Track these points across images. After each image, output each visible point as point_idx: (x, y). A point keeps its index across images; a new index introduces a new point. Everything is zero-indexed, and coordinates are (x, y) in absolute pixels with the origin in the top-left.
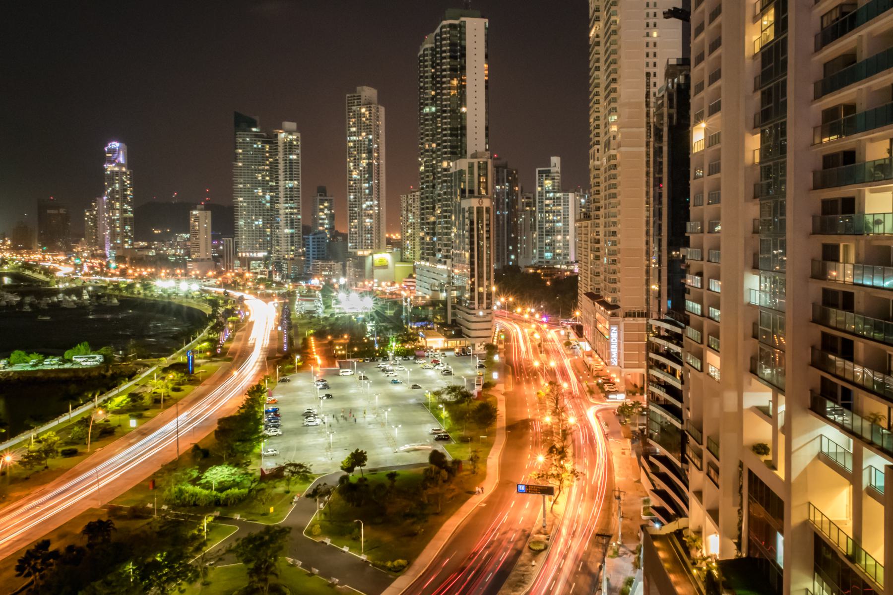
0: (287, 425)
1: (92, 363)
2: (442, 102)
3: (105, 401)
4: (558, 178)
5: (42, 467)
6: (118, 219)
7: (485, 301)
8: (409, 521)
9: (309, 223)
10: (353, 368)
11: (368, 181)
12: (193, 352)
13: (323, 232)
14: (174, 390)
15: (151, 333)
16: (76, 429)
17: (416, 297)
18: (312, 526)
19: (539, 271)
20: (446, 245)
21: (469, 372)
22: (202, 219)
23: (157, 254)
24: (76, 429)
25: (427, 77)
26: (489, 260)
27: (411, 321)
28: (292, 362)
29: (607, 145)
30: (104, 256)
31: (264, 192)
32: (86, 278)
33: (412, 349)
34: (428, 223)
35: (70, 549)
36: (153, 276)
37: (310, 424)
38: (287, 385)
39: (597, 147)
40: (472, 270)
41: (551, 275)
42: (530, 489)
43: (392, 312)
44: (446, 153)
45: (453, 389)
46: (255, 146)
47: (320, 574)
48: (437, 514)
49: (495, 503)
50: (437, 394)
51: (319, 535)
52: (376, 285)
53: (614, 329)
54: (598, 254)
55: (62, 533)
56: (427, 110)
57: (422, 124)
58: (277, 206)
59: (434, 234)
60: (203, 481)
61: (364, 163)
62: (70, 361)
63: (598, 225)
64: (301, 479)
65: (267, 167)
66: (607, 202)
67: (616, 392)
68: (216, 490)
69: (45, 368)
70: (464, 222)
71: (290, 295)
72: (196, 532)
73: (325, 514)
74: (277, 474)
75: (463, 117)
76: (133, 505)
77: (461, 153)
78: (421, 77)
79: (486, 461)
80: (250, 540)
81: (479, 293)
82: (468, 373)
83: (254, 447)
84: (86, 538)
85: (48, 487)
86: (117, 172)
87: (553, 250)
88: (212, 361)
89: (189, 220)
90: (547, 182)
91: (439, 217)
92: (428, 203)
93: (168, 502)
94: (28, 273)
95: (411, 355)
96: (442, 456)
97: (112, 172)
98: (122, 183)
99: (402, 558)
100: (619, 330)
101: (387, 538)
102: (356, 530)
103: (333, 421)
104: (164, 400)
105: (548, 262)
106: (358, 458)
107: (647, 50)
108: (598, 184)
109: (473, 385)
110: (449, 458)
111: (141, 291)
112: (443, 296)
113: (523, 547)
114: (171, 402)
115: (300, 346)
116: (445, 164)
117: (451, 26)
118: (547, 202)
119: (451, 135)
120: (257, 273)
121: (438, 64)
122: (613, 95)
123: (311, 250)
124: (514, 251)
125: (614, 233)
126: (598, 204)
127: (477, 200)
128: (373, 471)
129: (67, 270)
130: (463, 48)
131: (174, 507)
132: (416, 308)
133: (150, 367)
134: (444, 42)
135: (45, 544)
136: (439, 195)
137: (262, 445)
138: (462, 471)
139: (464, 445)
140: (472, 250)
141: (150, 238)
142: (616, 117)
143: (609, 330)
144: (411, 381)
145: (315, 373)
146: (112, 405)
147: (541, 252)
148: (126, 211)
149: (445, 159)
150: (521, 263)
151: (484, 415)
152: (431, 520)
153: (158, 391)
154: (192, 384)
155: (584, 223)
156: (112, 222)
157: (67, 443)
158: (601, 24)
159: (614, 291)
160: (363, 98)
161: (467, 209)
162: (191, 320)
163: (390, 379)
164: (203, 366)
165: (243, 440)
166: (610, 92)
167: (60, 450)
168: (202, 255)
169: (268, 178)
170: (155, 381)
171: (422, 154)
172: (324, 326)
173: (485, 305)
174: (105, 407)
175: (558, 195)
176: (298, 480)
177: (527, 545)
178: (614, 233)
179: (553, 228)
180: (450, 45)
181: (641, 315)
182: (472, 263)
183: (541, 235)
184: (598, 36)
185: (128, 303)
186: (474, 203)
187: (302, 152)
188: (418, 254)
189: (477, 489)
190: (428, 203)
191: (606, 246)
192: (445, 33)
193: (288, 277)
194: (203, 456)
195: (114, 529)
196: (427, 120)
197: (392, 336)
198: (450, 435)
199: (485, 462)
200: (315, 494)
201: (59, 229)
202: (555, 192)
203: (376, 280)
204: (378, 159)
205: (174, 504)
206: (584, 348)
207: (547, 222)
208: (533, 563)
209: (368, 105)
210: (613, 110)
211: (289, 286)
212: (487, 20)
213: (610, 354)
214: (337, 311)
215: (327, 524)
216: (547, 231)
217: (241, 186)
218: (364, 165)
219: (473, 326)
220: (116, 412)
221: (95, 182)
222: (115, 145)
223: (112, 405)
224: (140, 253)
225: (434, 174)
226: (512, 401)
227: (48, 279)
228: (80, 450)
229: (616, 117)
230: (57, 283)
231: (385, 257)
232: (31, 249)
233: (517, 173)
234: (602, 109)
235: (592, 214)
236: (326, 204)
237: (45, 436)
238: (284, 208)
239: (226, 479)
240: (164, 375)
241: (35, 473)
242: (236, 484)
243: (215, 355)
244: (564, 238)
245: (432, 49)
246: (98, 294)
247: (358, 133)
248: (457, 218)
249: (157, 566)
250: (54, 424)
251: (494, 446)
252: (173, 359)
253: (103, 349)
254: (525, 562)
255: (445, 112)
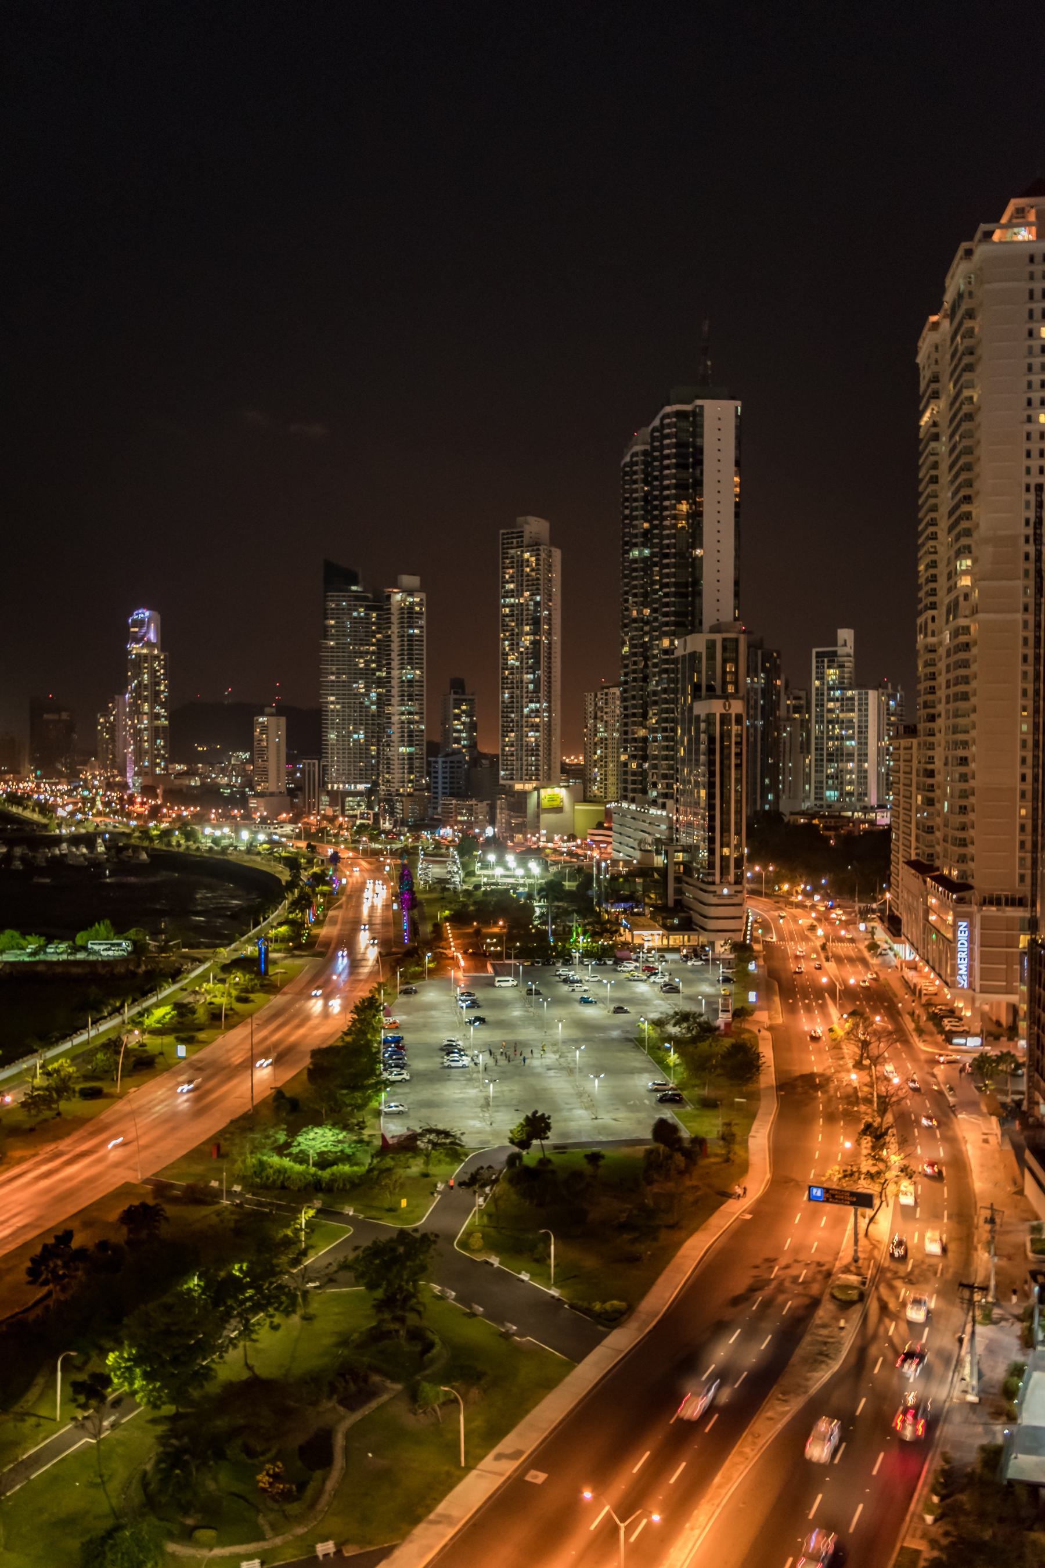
0: (419, 1065)
1: (116, 953)
2: (661, 540)
3: (141, 1014)
4: (849, 665)
5: (53, 1113)
6: (146, 729)
7: (732, 871)
8: (626, 1237)
9: (437, 739)
10: (516, 975)
11: (533, 669)
12: (267, 939)
13: (457, 752)
14: (241, 1000)
15: (199, 908)
16: (100, 1056)
17: (615, 862)
18: (469, 1234)
19: (816, 821)
20: (665, 776)
21: (706, 989)
22: (272, 729)
23: (203, 784)
24: (100, 1056)
25: (636, 500)
26: (738, 802)
27: (607, 901)
28: (419, 963)
29: (953, 609)
30: (124, 786)
31: (368, 687)
32: (98, 819)
33: (612, 947)
34: (635, 740)
35: (103, 1245)
36: (201, 819)
37: (453, 1064)
38: (413, 999)
39: (931, 613)
40: (712, 818)
41: (835, 828)
42: (832, 1196)
43: (575, 884)
44: (667, 624)
45: (683, 1018)
46: (355, 614)
47: (487, 1315)
48: (671, 1227)
49: (768, 1213)
50: (658, 1023)
51: (479, 1251)
52: (543, 839)
53: (963, 924)
54: (931, 795)
55: (87, 1217)
56: (636, 553)
57: (625, 576)
58: (389, 710)
59: (645, 758)
60: (295, 1150)
61: (527, 641)
62: (84, 948)
63: (931, 747)
64: (447, 1155)
65: (372, 648)
66: (950, 706)
67: (966, 1034)
68: (315, 1165)
69: (49, 958)
70: (698, 739)
71: (409, 853)
72: (289, 1233)
73: (490, 1216)
74: (408, 1145)
75: (696, 564)
76: (190, 1181)
77: (693, 624)
78: (626, 500)
79: (747, 1141)
80: (376, 1251)
81: (722, 857)
82: (707, 989)
83: (369, 1099)
84: (124, 1230)
85: (63, 1145)
86: (146, 656)
87: (839, 787)
88: (294, 956)
89: (253, 731)
90: (832, 671)
91: (654, 730)
92: (634, 706)
93: (242, 1179)
94: (14, 809)
95: (610, 957)
96: (674, 1129)
97: (138, 655)
98: (153, 672)
99: (620, 1299)
100: (971, 927)
101: (590, 1262)
102: (541, 1246)
103: (490, 1062)
104: (226, 1016)
105: (829, 806)
106: (536, 1126)
107: (1027, 446)
108: (933, 676)
109: (716, 1011)
110: (685, 1134)
111: (182, 842)
112: (659, 860)
113: (822, 1294)
114: (236, 1018)
115: (429, 937)
116: (666, 643)
117: (678, 414)
118: (831, 705)
119: (675, 594)
120: (355, 816)
121: (656, 478)
122: (964, 524)
123: (440, 780)
124: (773, 787)
125: (964, 761)
126: (931, 711)
127: (721, 702)
128: (561, 1148)
129: (77, 808)
130: (699, 451)
131: (249, 1186)
132: (614, 878)
133: (202, 961)
134: (667, 442)
135: (67, 1236)
136: (655, 693)
137: (383, 1096)
138: (707, 1156)
139: (709, 1113)
140: (711, 786)
141: (190, 758)
142: (969, 562)
143: (955, 927)
144: (612, 1000)
145: (457, 981)
146: (150, 1021)
147: (820, 788)
148: (157, 716)
149: (666, 634)
150: (785, 807)
151: (742, 1063)
152: (664, 1235)
153: (217, 1001)
154: (266, 992)
155: (904, 742)
156: (138, 732)
157: (86, 1078)
158: (942, 403)
159: (962, 859)
160: (527, 535)
161: (703, 717)
162: (253, 889)
163: (577, 996)
164: (282, 963)
165: (354, 1088)
166: (960, 518)
167: (78, 1087)
168: (272, 786)
169: (374, 665)
170: (211, 985)
171: (626, 626)
172: (465, 905)
173: (731, 878)
174: (141, 1023)
175: (849, 693)
176: (442, 1157)
177: (828, 1291)
178: (964, 761)
179: (840, 750)
180: (677, 445)
181: (1020, 902)
182: (711, 807)
183: (819, 761)
184: (935, 424)
185: (165, 860)
186: (717, 707)
187: (428, 622)
188: (612, 790)
189: (739, 1191)
190: (634, 706)
191: (947, 782)
192: (669, 426)
193: (403, 823)
194: (290, 1110)
195: (167, 1219)
196: (635, 570)
197: (576, 924)
198: (685, 1094)
199: (745, 1142)
200: (474, 1181)
201: (63, 743)
202: (843, 689)
203: (544, 832)
204: (549, 633)
205: (252, 1185)
206: (901, 954)
207: (830, 738)
208: (842, 1323)
209: (534, 546)
210: (964, 551)
211: (406, 840)
212: (738, 403)
213: (955, 969)
214: (485, 880)
215: (492, 1232)
216: (830, 754)
217: (333, 678)
218: (527, 643)
219: (713, 912)
220: (154, 1032)
221: (113, 672)
222: (144, 614)
223: (150, 1021)
224: (178, 782)
225: (646, 659)
226: (783, 1040)
227: (45, 821)
228: (106, 1090)
229: (969, 562)
230: (59, 826)
231: (558, 794)
232: (19, 773)
233: (779, 656)
234: (941, 549)
235: (921, 727)
236: (464, 707)
237: (56, 1065)
238: (398, 711)
239: (330, 1148)
240: (223, 976)
241: (40, 1124)
242: (345, 1158)
243: (299, 947)
244: (860, 766)
245: (645, 453)
246: (117, 844)
247: (517, 593)
248: (686, 731)
249: (235, 1285)
250: (67, 1046)
251: (759, 1116)
252: (235, 950)
253: (133, 931)
254: (826, 1320)
255: (667, 556)
